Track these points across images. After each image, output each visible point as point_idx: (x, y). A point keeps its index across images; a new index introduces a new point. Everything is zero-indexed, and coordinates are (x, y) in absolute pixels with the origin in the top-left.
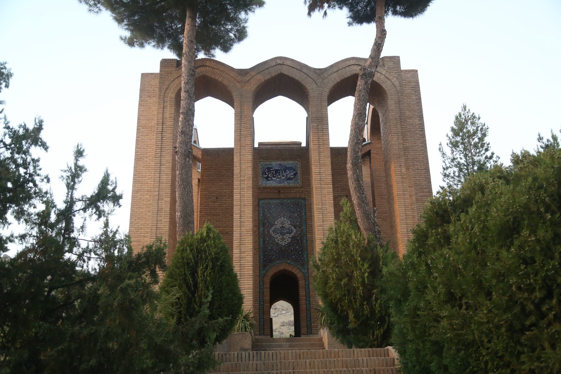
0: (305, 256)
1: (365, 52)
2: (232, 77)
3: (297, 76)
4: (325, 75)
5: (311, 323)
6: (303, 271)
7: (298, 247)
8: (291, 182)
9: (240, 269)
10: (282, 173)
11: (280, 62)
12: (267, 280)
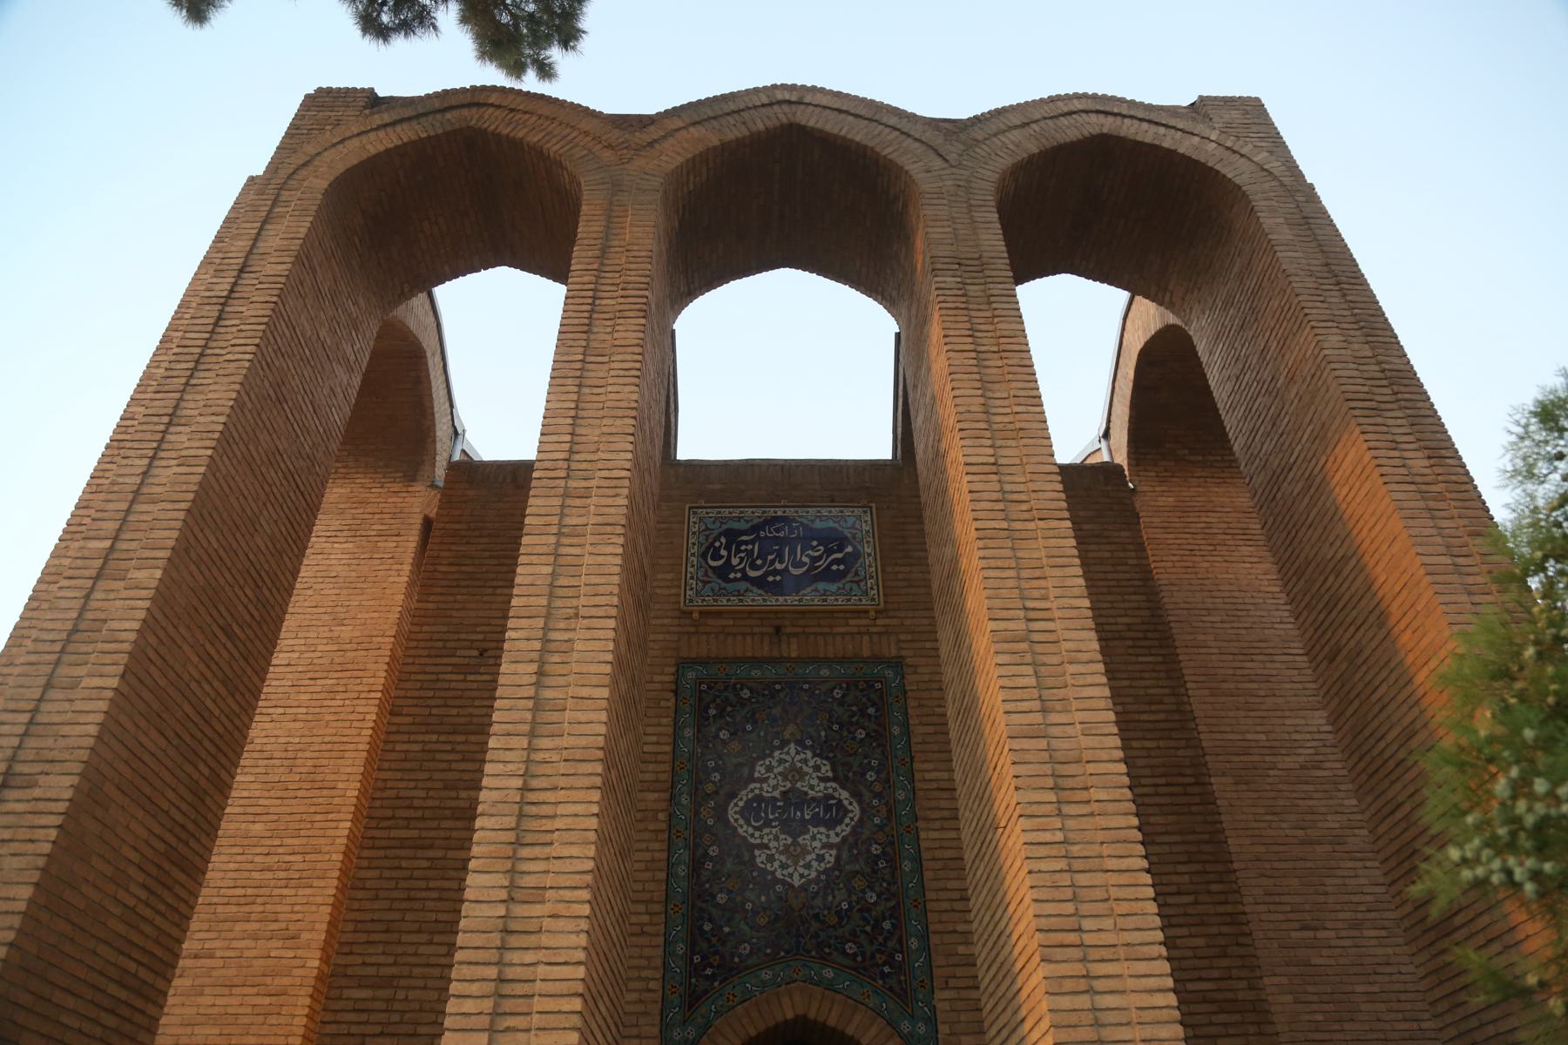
0: (914, 943)
2: (586, 133)
3: (858, 133)
6: (906, 1026)
7: (872, 897)
8: (833, 587)
9: (496, 1014)
10: (793, 552)
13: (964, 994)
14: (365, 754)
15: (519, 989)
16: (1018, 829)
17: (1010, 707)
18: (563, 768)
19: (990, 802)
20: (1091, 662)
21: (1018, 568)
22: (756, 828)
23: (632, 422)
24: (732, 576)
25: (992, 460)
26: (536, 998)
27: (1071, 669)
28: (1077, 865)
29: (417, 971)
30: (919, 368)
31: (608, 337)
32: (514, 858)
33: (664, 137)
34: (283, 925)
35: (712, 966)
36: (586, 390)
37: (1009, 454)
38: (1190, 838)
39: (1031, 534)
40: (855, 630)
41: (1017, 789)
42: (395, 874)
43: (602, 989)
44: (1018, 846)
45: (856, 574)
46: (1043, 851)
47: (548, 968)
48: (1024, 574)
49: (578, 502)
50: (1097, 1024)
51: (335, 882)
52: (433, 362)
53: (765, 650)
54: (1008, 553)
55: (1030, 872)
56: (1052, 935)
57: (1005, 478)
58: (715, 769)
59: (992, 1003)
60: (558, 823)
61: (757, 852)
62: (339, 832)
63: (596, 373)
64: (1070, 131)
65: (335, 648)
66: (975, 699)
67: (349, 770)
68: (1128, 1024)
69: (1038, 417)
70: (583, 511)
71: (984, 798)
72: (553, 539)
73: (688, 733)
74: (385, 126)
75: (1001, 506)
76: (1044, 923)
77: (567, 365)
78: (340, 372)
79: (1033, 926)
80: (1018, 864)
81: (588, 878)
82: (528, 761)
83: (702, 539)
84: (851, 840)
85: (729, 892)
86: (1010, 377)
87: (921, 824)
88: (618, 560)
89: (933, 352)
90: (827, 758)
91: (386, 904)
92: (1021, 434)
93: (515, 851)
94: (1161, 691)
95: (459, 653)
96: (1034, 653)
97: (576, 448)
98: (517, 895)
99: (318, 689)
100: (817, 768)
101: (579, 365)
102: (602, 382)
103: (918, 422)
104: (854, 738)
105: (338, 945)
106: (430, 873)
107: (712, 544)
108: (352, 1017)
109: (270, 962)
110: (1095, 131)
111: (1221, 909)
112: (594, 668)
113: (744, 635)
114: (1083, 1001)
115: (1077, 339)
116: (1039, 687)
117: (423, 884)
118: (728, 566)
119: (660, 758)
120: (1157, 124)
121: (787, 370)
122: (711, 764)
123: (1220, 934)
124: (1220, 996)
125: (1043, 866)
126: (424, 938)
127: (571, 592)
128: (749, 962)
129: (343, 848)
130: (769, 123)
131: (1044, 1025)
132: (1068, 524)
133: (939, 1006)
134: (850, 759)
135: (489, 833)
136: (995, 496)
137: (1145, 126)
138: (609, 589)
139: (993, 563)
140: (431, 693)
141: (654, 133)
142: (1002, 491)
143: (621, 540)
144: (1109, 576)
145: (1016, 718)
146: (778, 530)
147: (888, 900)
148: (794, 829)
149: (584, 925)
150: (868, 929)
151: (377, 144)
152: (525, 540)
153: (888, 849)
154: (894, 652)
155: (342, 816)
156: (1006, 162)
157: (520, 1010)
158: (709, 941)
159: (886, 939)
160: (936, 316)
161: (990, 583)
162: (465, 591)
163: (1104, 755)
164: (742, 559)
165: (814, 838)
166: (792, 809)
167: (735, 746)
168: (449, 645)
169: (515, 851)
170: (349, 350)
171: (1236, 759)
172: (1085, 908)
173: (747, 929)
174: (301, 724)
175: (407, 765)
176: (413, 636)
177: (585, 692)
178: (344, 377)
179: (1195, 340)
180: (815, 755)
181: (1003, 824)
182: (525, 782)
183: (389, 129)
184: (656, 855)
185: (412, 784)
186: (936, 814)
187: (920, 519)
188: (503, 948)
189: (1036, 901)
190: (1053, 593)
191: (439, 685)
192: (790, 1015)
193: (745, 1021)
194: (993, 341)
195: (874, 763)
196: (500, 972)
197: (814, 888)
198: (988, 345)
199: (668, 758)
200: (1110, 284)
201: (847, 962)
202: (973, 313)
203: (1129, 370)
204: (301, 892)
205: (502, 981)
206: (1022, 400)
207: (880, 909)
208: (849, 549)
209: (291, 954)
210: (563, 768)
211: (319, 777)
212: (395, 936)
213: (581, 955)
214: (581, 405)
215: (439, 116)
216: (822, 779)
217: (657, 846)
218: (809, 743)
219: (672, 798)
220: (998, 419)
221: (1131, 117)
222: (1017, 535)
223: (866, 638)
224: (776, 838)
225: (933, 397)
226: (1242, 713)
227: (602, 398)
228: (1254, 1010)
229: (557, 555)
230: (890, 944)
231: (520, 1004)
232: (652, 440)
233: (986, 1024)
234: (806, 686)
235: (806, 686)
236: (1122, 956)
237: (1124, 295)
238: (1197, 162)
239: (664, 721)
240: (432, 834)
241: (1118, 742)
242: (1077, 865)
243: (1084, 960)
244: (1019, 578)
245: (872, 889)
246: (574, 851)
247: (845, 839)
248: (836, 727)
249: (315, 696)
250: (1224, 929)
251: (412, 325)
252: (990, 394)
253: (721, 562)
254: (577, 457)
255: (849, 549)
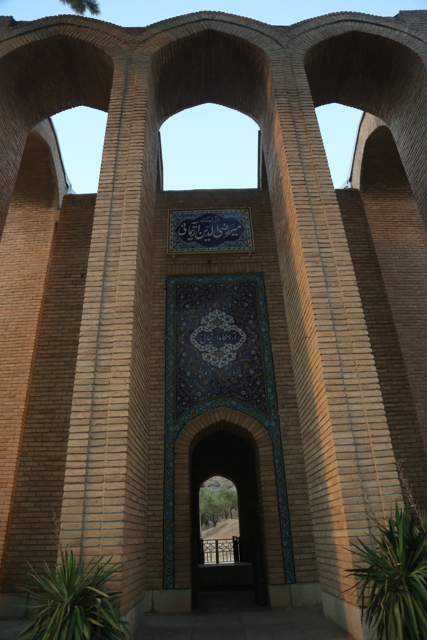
0: (270, 390)
2: (114, 37)
3: (240, 33)
5: (292, 554)
7: (252, 372)
8: (233, 243)
9: (92, 418)
10: (215, 229)
12: (184, 446)
13: (291, 410)
14: (37, 322)
15: (101, 408)
16: (316, 336)
17: (312, 285)
18: (116, 315)
19: (303, 327)
20: (348, 265)
21: (315, 226)
22: (202, 345)
23: (141, 166)
24: (189, 239)
25: (303, 179)
26: (109, 412)
27: (339, 268)
28: (342, 351)
29: (62, 407)
30: (269, 144)
31: (129, 129)
32: (96, 354)
33: (150, 38)
34: (9, 392)
35: (185, 401)
36: (119, 153)
37: (311, 176)
38: (386, 345)
39: (320, 211)
40: (243, 261)
41: (315, 319)
42: (51, 368)
43: (137, 408)
44: (316, 344)
45: (243, 237)
46: (327, 346)
47: (113, 399)
48: (318, 228)
49: (118, 201)
50: (350, 417)
51: (29, 375)
52: (54, 154)
53: (204, 270)
54: (311, 219)
55: (321, 355)
56: (331, 380)
57: (309, 187)
58: (184, 321)
59: (303, 411)
60: (115, 339)
61: (203, 355)
62: (28, 355)
63: (124, 145)
64: (339, 30)
65: (21, 279)
66: (296, 285)
67: (31, 329)
68: (363, 416)
69: (324, 160)
70: (120, 205)
71: (300, 326)
72: (108, 218)
73: (172, 306)
74: (20, 35)
75: (307, 199)
76: (327, 375)
77: (111, 142)
78: (10, 153)
79: (323, 377)
80: (316, 351)
81: (129, 361)
82: (101, 313)
83: (175, 224)
84: (243, 349)
85: (192, 371)
86: (311, 142)
87: (272, 342)
88: (137, 226)
89: (276, 134)
90: (232, 315)
91: (48, 381)
92: (316, 167)
93: (97, 351)
94: (374, 285)
95: (72, 276)
96: (322, 262)
97: (116, 178)
98: (99, 369)
99: (16, 296)
100: (227, 319)
101: (116, 142)
102: (127, 149)
103: (269, 169)
104: (243, 307)
105: (30, 398)
106: (66, 367)
107: (180, 226)
108: (37, 426)
109: (4, 407)
110: (351, 29)
111: (398, 374)
112: (128, 273)
113: (195, 264)
114: (344, 408)
115: (341, 130)
116: (325, 276)
117: (63, 372)
118: (187, 235)
119: (161, 317)
120: (379, 25)
121: (210, 149)
122: (182, 319)
123: (398, 384)
124: (397, 409)
125: (327, 352)
126: (65, 393)
127: (117, 240)
128: (201, 399)
129: (31, 361)
130: (199, 30)
131: (327, 418)
132: (337, 206)
133: (281, 415)
134: (242, 315)
135: (85, 344)
136: (305, 194)
137: (374, 26)
138: (133, 238)
139: (304, 223)
140: (61, 293)
141: (145, 35)
142: (308, 192)
143: (138, 217)
144: (352, 237)
145: (315, 290)
146: (208, 220)
147: (258, 373)
148: (219, 345)
149: (128, 381)
150: (250, 385)
151: (17, 43)
152: (95, 219)
153: (258, 352)
154: (260, 270)
155: (29, 348)
156: (308, 45)
157: (102, 416)
158: (184, 391)
159: (258, 389)
160: (277, 116)
161: (303, 232)
162: (74, 250)
163: (353, 305)
164: (193, 232)
165: (227, 348)
166: (217, 337)
167: (192, 311)
168: (68, 273)
169: (97, 351)
170: (14, 144)
171: (404, 315)
172: (345, 369)
173: (200, 386)
174: (9, 311)
175: (53, 324)
176: (52, 270)
177: (125, 283)
178: (13, 157)
179: (392, 132)
180: (227, 314)
181: (309, 336)
182: (100, 322)
183: (22, 37)
184: (160, 357)
185: (56, 331)
186: (279, 337)
187: (270, 213)
188: (93, 391)
189: (324, 366)
190: (330, 236)
191: (65, 290)
192: (218, 420)
193: (200, 423)
194: (303, 127)
195: (252, 317)
196: (93, 401)
197: (227, 368)
198: (301, 128)
199: (164, 317)
200: (355, 107)
201: (242, 398)
202: (294, 115)
203: (361, 150)
204: (15, 379)
205: (94, 405)
206: (317, 153)
207: (255, 376)
208: (240, 227)
209: (13, 403)
210: (116, 315)
211: (19, 332)
212: (52, 393)
213: (127, 393)
214: (118, 159)
215: (45, 30)
216: (229, 324)
217: (160, 353)
218: (224, 309)
219: (166, 333)
220: (306, 161)
221: (368, 22)
222: (315, 211)
223: (248, 264)
224: (211, 348)
225: (276, 155)
226: (407, 297)
227: (127, 156)
228: (411, 415)
229: (110, 225)
230: (260, 391)
231: (102, 415)
232: (151, 178)
233: (301, 421)
234: (222, 285)
235: (222, 285)
236: (361, 389)
237: (361, 112)
238: (398, 43)
239: (162, 301)
240: (65, 351)
241: (360, 299)
242: (342, 351)
243: (344, 391)
244: (315, 230)
245: (252, 369)
246: (122, 350)
247: (240, 348)
248: (235, 302)
249: (14, 299)
250: (399, 382)
251: (43, 136)
252: (302, 150)
253: (184, 234)
254: (117, 182)
255: (240, 227)
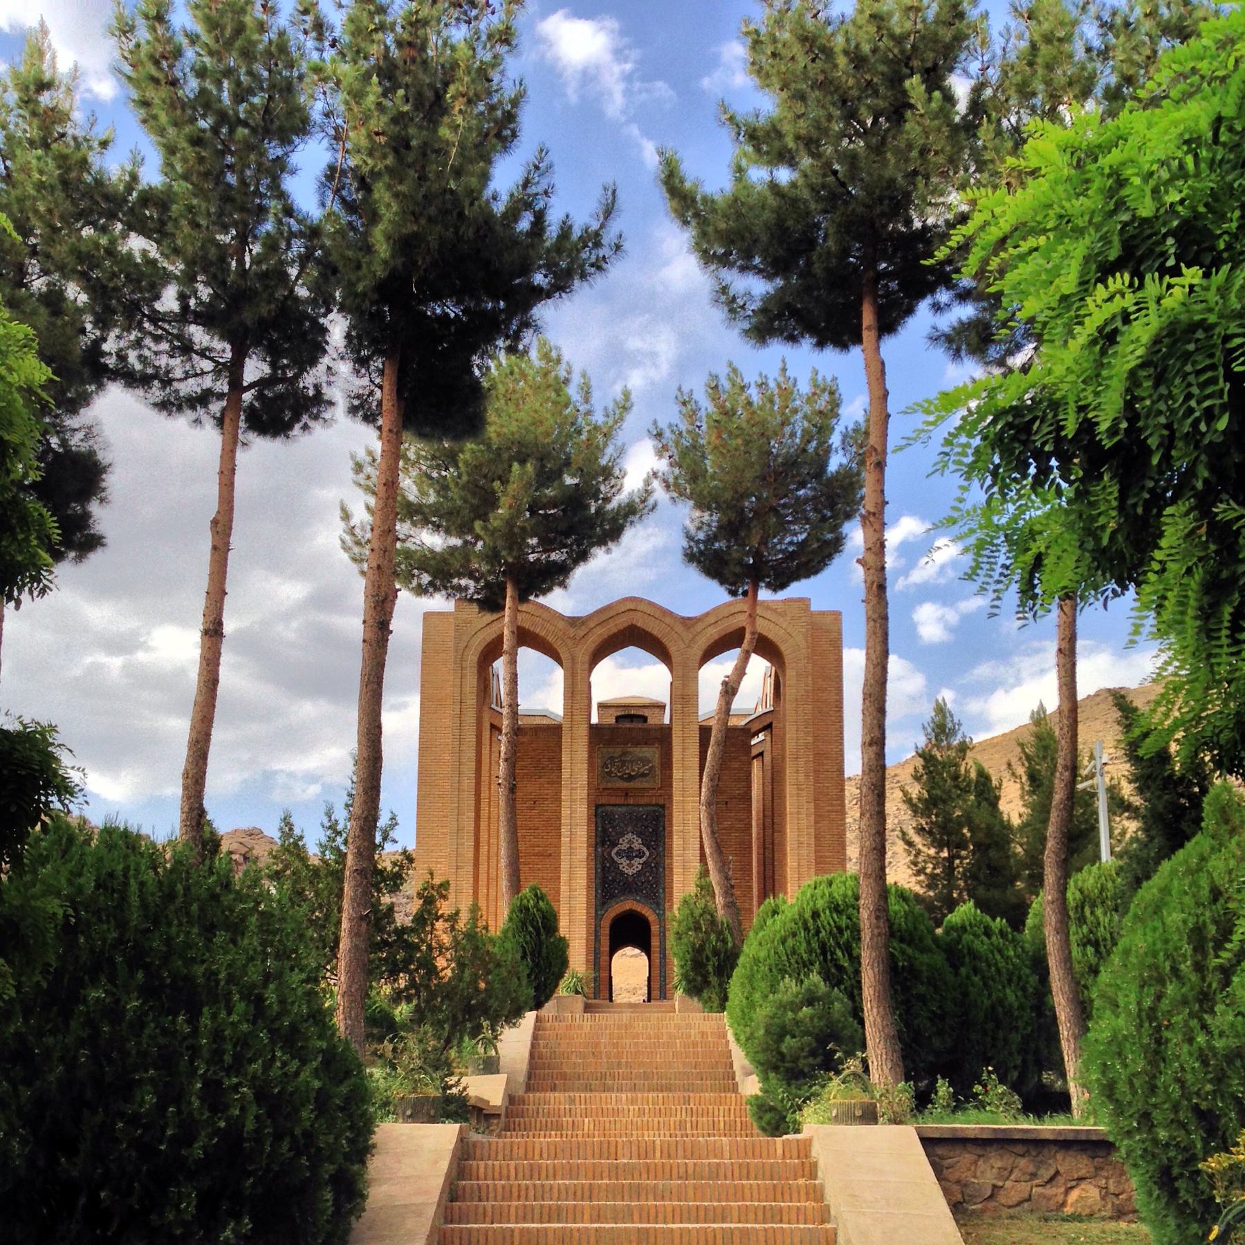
1: (1052, 702)
4: (699, 627)
11: (633, 604)
12: (606, 924)
